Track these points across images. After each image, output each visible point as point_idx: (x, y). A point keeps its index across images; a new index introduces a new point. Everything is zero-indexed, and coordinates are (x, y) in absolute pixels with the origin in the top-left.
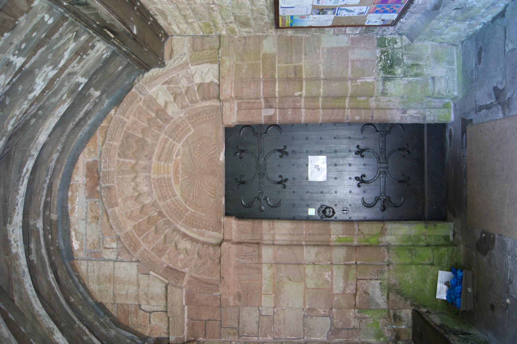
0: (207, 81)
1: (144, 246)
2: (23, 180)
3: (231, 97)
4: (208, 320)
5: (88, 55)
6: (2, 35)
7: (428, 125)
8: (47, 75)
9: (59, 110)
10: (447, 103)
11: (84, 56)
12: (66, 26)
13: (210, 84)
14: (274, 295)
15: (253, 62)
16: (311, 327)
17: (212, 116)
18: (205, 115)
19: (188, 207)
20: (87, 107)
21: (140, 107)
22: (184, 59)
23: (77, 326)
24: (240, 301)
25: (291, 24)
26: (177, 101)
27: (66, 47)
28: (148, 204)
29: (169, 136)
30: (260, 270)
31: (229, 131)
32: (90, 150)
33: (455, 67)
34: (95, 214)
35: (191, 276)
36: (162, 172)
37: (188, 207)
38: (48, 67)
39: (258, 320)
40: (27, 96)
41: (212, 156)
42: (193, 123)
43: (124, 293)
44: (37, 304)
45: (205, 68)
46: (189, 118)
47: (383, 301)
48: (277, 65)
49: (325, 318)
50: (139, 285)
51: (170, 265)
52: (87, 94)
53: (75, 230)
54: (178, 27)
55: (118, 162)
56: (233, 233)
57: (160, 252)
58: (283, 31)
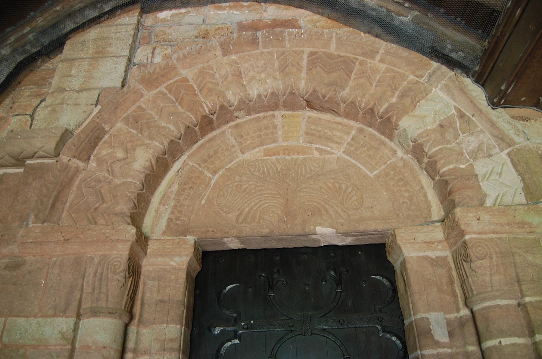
1: (149, 95)
19: (220, 173)
22: (517, 139)
32: (318, 21)
34: (211, 33)
35: (77, 171)
41: (324, 213)
42: (387, 174)
43: (73, 72)
50: (81, 91)
56: (160, 259)
57: (135, 121)
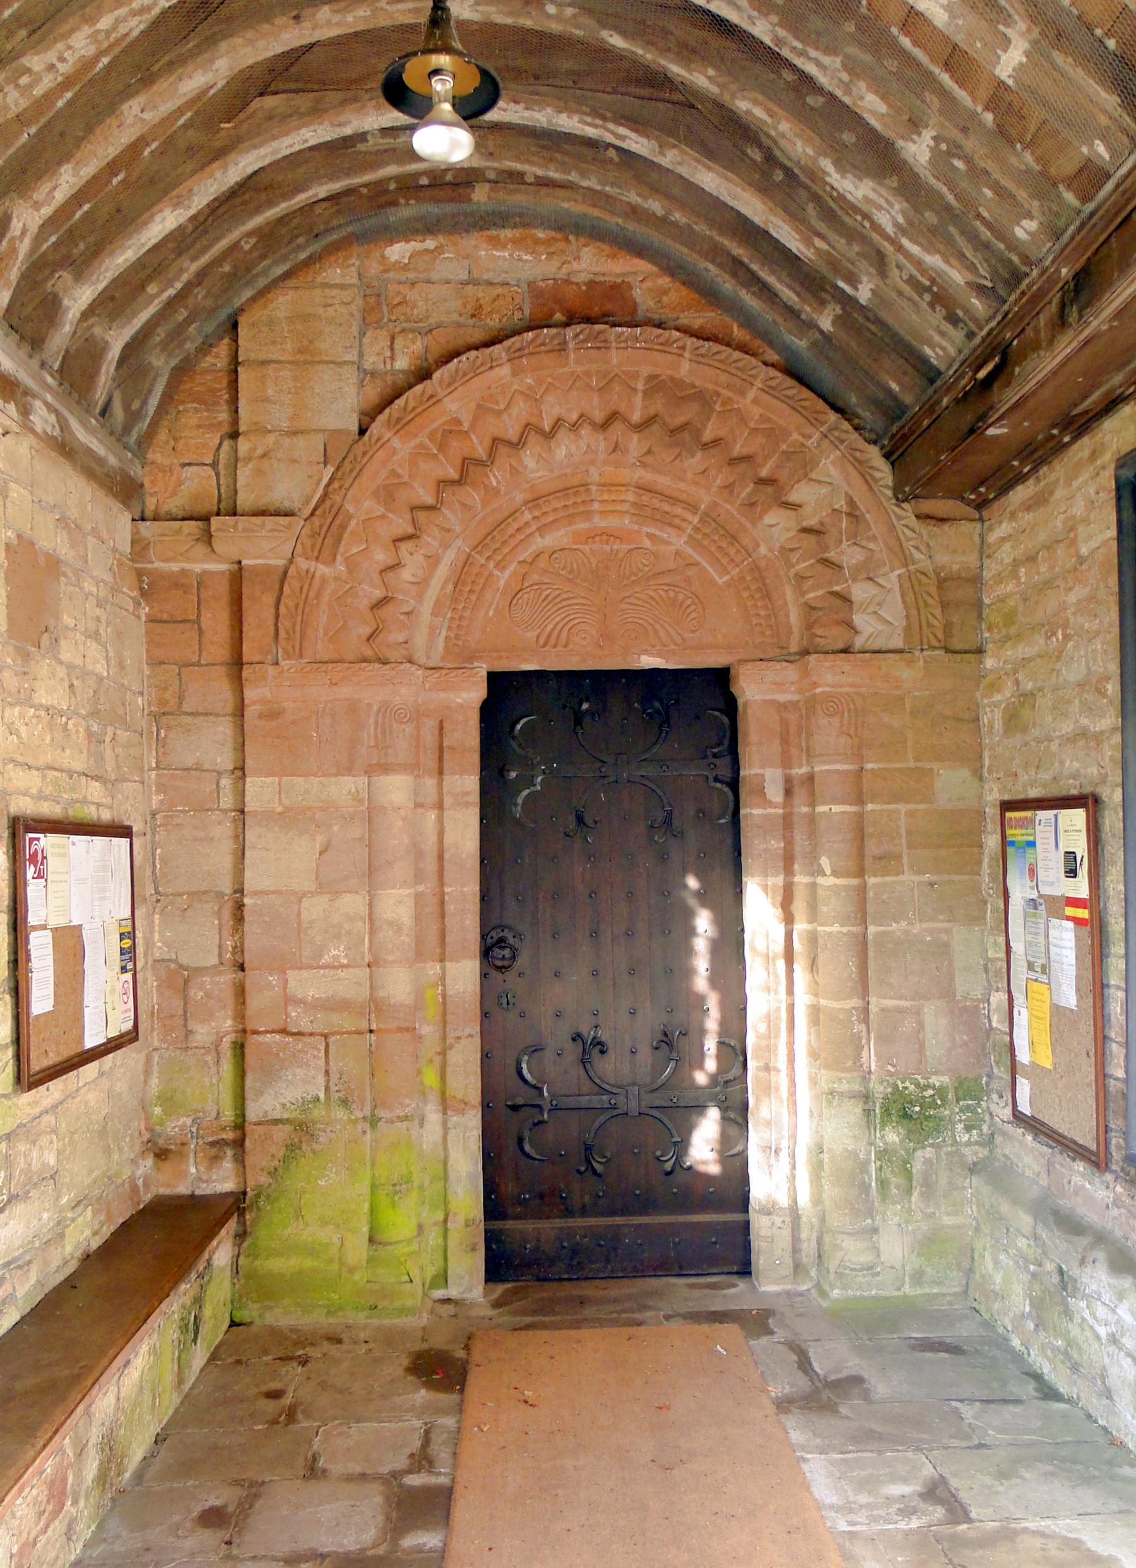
0: (858, 619)
2: (596, 126)
3: (815, 685)
4: (200, 629)
5: (932, 305)
6: (987, 108)
7: (747, 1223)
8: (880, 208)
9: (786, 227)
10: (808, 1273)
11: (927, 297)
12: (1010, 261)
13: (850, 625)
14: (280, 809)
15: (910, 743)
16: (189, 913)
17: (763, 633)
18: (763, 613)
19: (512, 568)
20: (787, 294)
21: (786, 433)
22: (917, 555)
23: (186, 264)
24: (260, 717)
25: (1013, 843)
26: (803, 535)
27: (954, 262)
28: (520, 461)
29: (706, 514)
30: (349, 770)
31: (717, 683)
32: (665, 292)
33: (907, 1289)
36: (605, 497)
37: (512, 568)
38: (903, 212)
39: (206, 766)
40: (826, 155)
44: (256, 160)
45: (894, 612)
46: (755, 568)
47: (268, 1108)
48: (902, 808)
49: (216, 951)
51: (353, 523)
52: (824, 295)
53: (439, 249)
54: (1003, 539)
55: (635, 376)
56: (442, 695)
58: (993, 822)
